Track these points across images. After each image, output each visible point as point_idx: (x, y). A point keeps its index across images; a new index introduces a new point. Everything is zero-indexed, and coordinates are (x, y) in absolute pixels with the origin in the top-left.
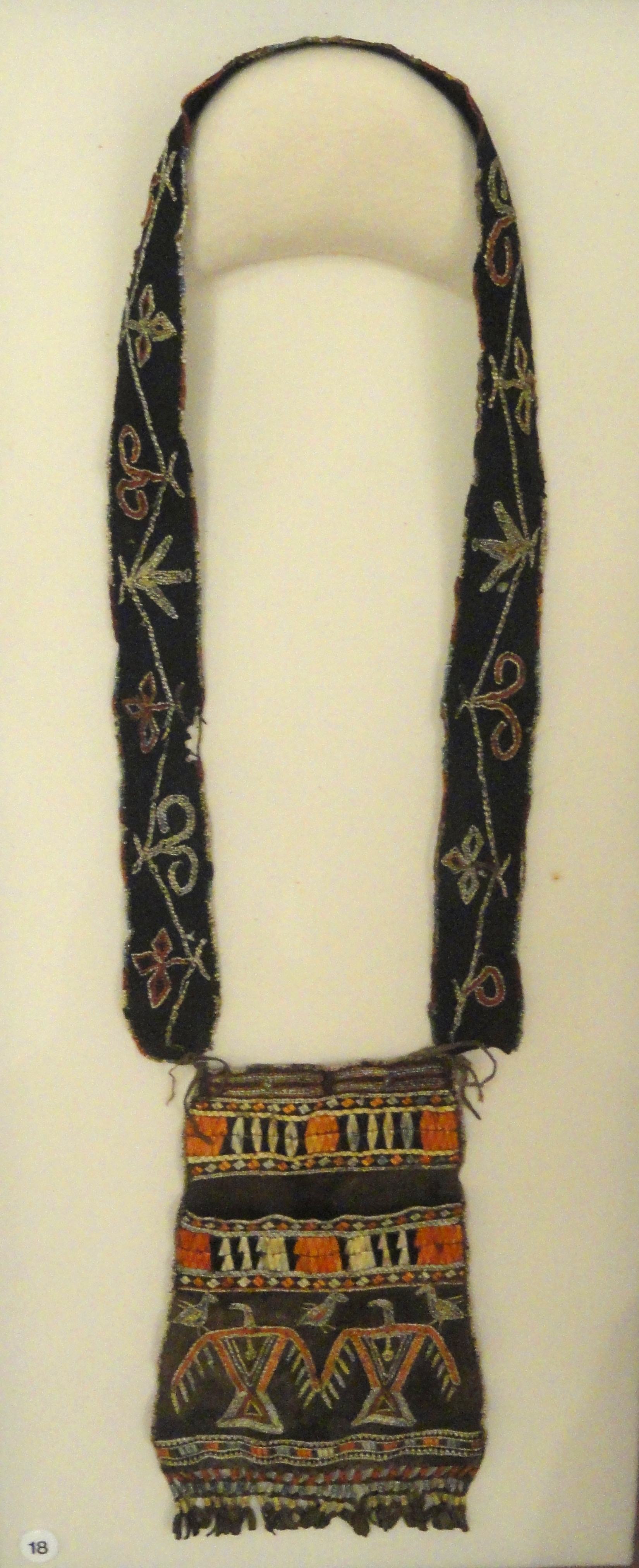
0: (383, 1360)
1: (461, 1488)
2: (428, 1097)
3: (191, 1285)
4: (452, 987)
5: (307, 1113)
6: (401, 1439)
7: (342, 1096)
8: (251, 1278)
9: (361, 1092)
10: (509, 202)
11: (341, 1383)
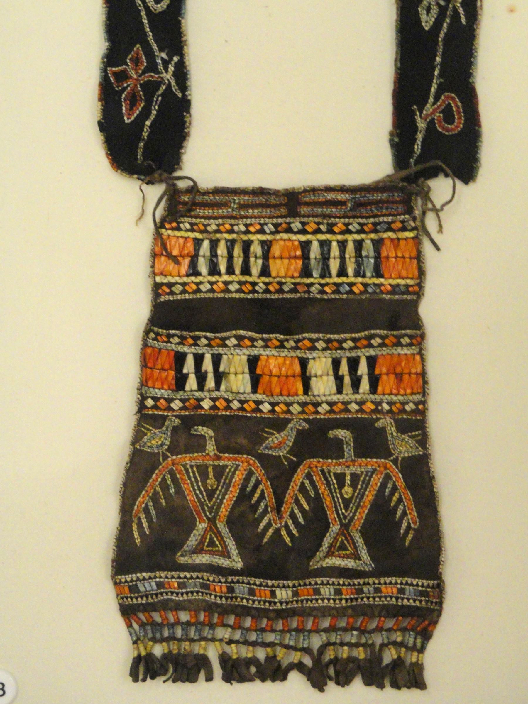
1: (419, 644)
2: (389, 223)
4: (414, 114)
5: (272, 233)
8: (214, 400)
9: (324, 216)
11: (301, 520)
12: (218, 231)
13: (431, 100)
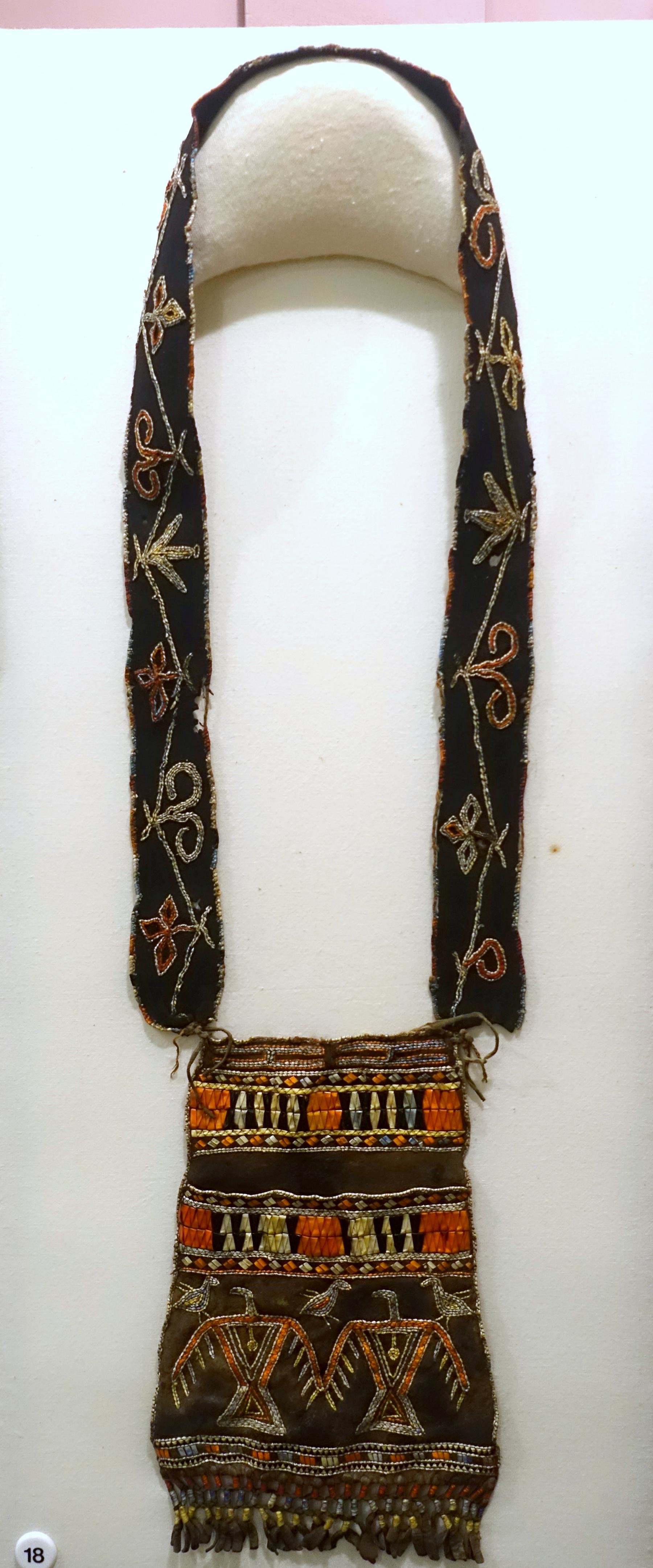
0: (388, 1359)
3: (192, 1266)
6: (408, 1450)
7: (344, 1071)
9: (363, 1066)
10: (491, 192)
12: (254, 1083)
13: (472, 946)
